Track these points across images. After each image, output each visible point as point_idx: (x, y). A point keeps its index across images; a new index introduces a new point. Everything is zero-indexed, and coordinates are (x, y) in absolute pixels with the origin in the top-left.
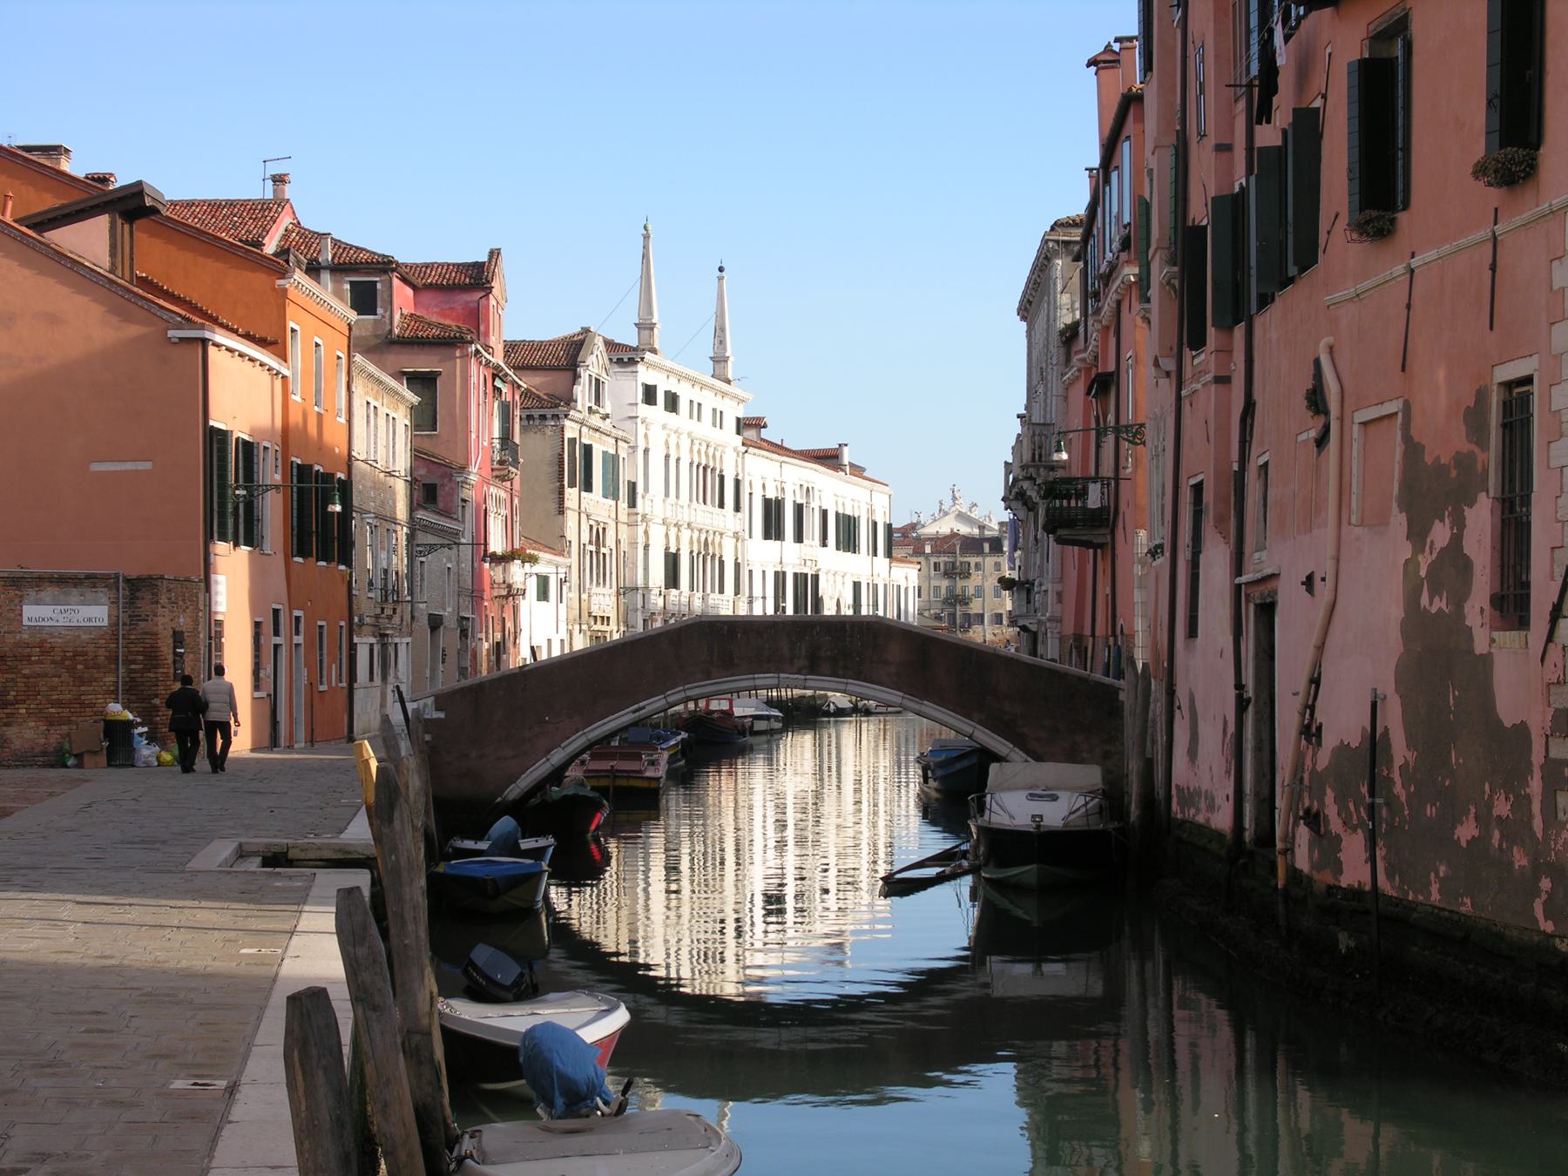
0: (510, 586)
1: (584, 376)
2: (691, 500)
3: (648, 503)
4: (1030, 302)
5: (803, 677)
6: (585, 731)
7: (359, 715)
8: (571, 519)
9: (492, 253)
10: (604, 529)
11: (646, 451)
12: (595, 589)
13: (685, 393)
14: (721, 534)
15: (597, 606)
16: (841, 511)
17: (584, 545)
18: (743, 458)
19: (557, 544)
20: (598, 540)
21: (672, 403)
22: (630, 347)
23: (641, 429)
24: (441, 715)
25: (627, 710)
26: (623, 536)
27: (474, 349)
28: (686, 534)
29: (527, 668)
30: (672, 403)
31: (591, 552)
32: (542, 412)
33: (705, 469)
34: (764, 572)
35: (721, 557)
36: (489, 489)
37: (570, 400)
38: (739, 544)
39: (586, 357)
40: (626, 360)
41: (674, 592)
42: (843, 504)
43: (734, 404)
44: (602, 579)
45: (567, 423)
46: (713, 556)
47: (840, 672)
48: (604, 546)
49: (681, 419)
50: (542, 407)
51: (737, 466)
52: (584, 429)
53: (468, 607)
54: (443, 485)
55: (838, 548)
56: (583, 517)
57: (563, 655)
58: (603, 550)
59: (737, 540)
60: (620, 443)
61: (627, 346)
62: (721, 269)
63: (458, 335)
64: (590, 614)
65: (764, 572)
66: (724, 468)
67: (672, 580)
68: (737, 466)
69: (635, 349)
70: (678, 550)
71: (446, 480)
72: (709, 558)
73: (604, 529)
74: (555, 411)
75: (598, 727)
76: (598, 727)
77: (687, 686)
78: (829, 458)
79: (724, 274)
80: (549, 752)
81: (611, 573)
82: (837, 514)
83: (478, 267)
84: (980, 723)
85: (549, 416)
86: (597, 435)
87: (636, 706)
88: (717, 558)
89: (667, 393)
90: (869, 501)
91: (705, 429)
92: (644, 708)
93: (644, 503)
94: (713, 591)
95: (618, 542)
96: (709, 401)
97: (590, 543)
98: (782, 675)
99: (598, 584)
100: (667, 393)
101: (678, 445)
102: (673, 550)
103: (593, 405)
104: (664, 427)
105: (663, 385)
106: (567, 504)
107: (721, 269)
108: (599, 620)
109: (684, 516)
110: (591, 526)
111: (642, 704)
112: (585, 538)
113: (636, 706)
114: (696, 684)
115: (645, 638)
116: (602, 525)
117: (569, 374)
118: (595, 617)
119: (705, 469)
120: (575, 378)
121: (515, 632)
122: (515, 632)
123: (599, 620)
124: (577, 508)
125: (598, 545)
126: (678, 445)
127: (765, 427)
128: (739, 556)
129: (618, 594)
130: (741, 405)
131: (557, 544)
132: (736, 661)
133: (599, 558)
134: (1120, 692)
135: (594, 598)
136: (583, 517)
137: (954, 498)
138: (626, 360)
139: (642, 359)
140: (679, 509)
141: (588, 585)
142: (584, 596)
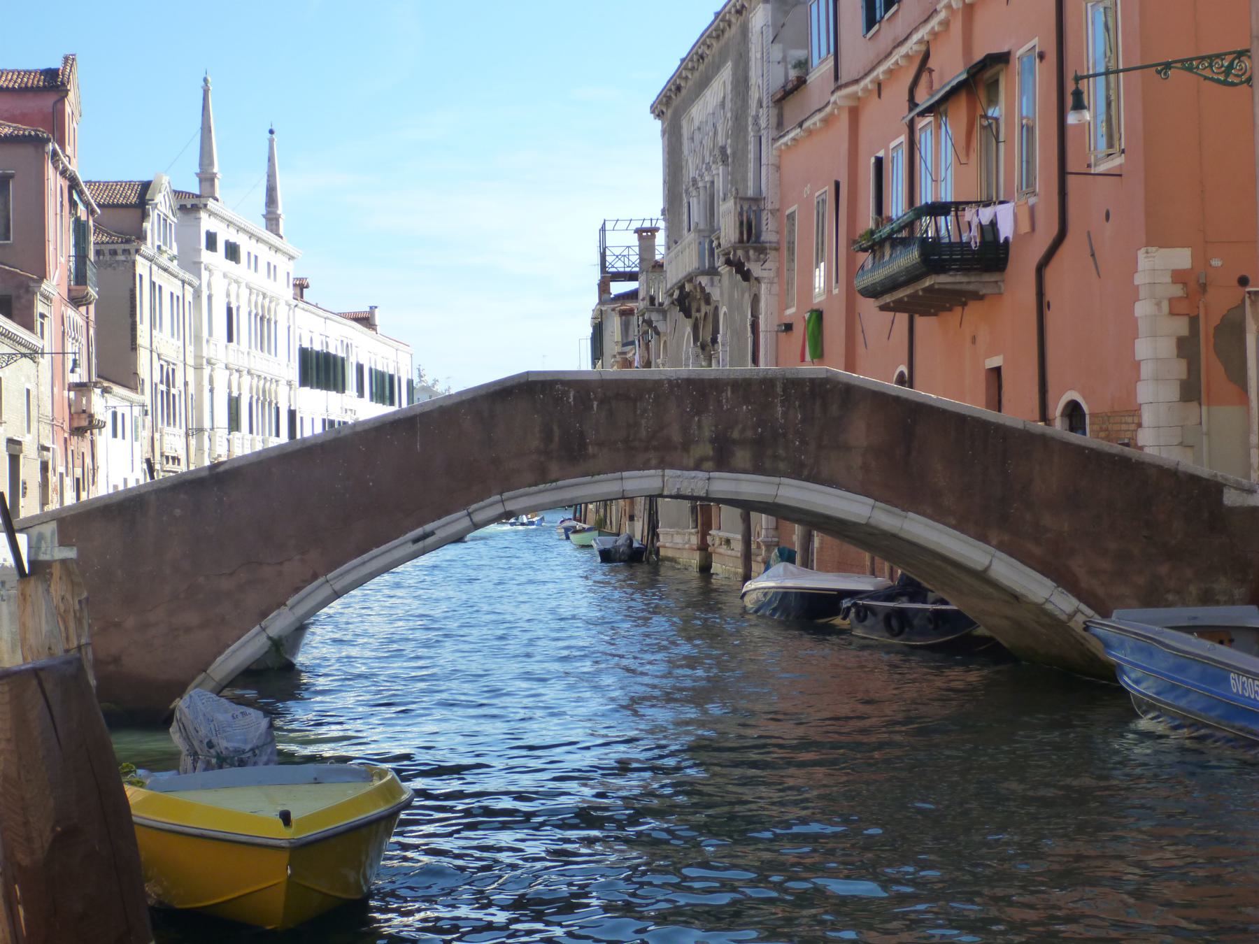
0: (91, 416)
1: (153, 215)
2: (250, 347)
3: (212, 347)
4: (679, 88)
5: (705, 475)
6: (330, 576)
7: (6, 389)
8: (143, 357)
9: (66, 59)
10: (173, 370)
11: (210, 297)
12: (167, 429)
13: (245, 245)
14: (277, 381)
15: (169, 446)
16: (373, 367)
17: (156, 385)
18: (294, 312)
19: (130, 380)
20: (168, 380)
21: (232, 252)
22: (193, 194)
23: (205, 274)
24: (70, 553)
25: (402, 539)
26: (191, 378)
27: (51, 148)
28: (246, 380)
29: (221, 469)
30: (232, 252)
31: (162, 392)
32: (112, 247)
33: (262, 319)
34: (313, 419)
35: (276, 404)
36: (66, 310)
37: (141, 237)
38: (292, 392)
39: (154, 194)
40: (189, 206)
41: (236, 434)
42: (375, 362)
43: (285, 259)
44: (171, 418)
45: (138, 258)
46: (270, 404)
47: (768, 464)
48: (174, 387)
49: (239, 270)
50: (113, 243)
51: (289, 319)
52: (155, 268)
53: (48, 436)
54: (19, 297)
55: (371, 400)
56: (155, 356)
57: (314, 436)
58: (173, 391)
59: (291, 388)
60: (186, 286)
61: (189, 194)
62: (271, 132)
63: (33, 133)
64: (162, 455)
65: (313, 419)
66: (277, 319)
67: (234, 424)
68: (289, 319)
69: (198, 196)
70: (240, 395)
71: (22, 291)
72: (267, 403)
73: (173, 370)
74: (127, 246)
75: (354, 568)
76: (354, 568)
77: (506, 495)
78: (366, 320)
79: (274, 136)
80: (264, 615)
81: (180, 415)
82: (371, 370)
83: (51, 74)
84: (1001, 547)
85: (120, 252)
86: (166, 274)
87: (418, 532)
88: (273, 405)
89: (227, 243)
90: (395, 359)
91: (260, 279)
92: (432, 533)
93: (208, 348)
94: (270, 434)
95: (186, 384)
96: (265, 254)
97: (162, 382)
98: (668, 472)
99: (169, 424)
100: (227, 243)
101: (238, 296)
102: (235, 394)
103: (161, 244)
104: (225, 276)
105: (225, 235)
106: (140, 341)
107: (271, 132)
108: (171, 461)
109: (243, 362)
110: (162, 366)
111: (428, 527)
112: (157, 378)
113: (418, 532)
114: (522, 491)
115: (431, 411)
116: (171, 366)
117: (138, 212)
118: (167, 458)
119: (262, 319)
120: (144, 216)
121: (94, 469)
122: (94, 469)
123: (171, 461)
124: (149, 346)
125: (168, 385)
126: (238, 296)
127: (307, 287)
128: (292, 403)
129: (187, 435)
130: (291, 262)
131: (130, 380)
132: (590, 450)
133: (169, 399)
134: (1226, 490)
135: (166, 437)
136: (155, 356)
137: (420, 376)
138: (189, 206)
139: (205, 205)
140: (240, 355)
141: (160, 425)
142: (157, 436)
